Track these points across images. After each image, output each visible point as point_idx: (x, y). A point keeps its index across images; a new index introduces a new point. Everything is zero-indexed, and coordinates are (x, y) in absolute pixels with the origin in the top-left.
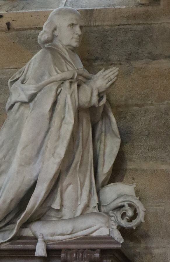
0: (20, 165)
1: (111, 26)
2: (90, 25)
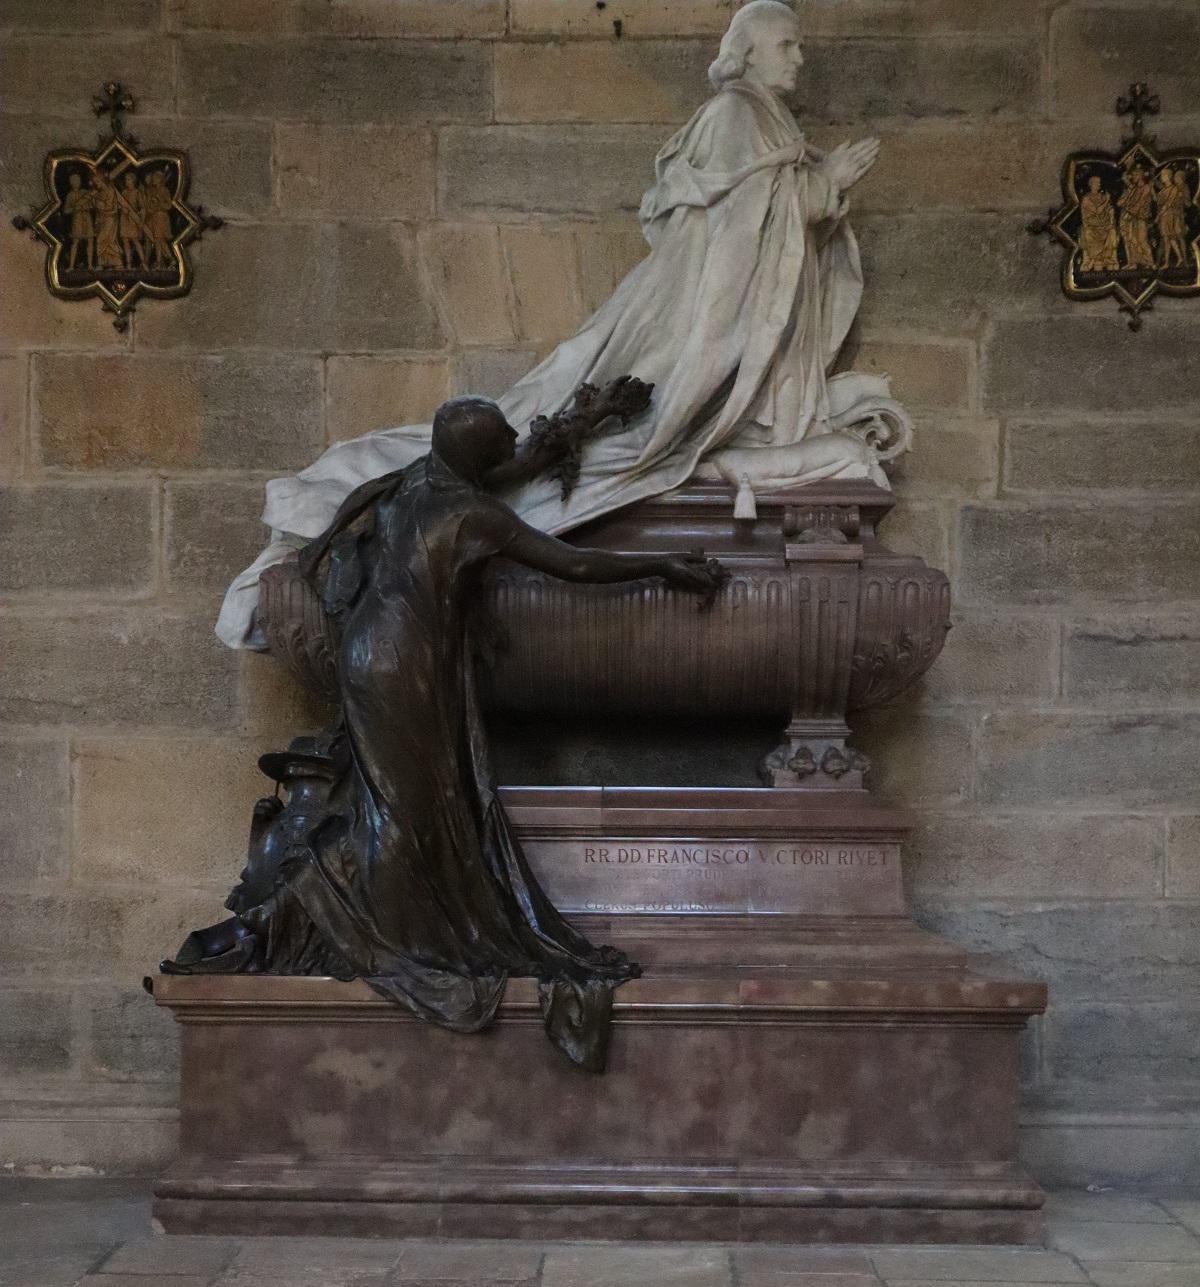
0: (708, 339)
1: (832, 39)
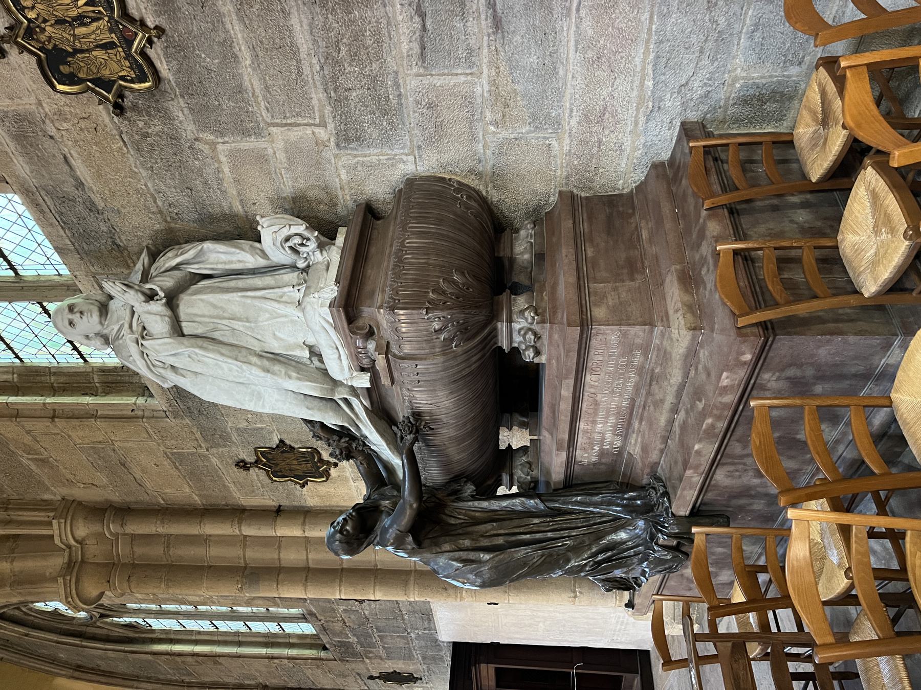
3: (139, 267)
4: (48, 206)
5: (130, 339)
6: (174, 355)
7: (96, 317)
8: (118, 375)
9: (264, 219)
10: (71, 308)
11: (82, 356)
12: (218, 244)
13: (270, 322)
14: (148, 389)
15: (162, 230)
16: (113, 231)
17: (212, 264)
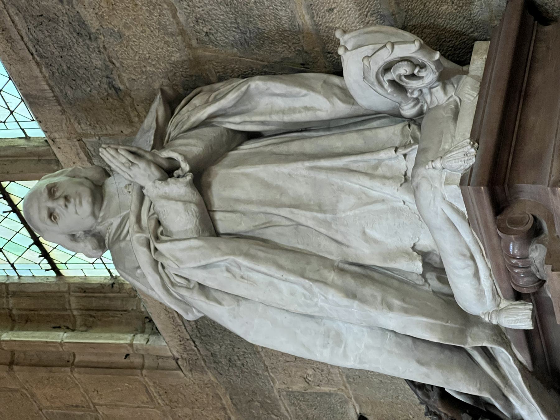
2: (54, 98)
3: (150, 122)
4: (19, 31)
5: (138, 238)
6: (204, 267)
7: (86, 207)
8: (105, 297)
9: (347, 36)
10: (51, 191)
11: (54, 267)
12: (273, 81)
13: (357, 212)
14: (151, 321)
15: (183, 62)
16: (111, 66)
17: (262, 114)
